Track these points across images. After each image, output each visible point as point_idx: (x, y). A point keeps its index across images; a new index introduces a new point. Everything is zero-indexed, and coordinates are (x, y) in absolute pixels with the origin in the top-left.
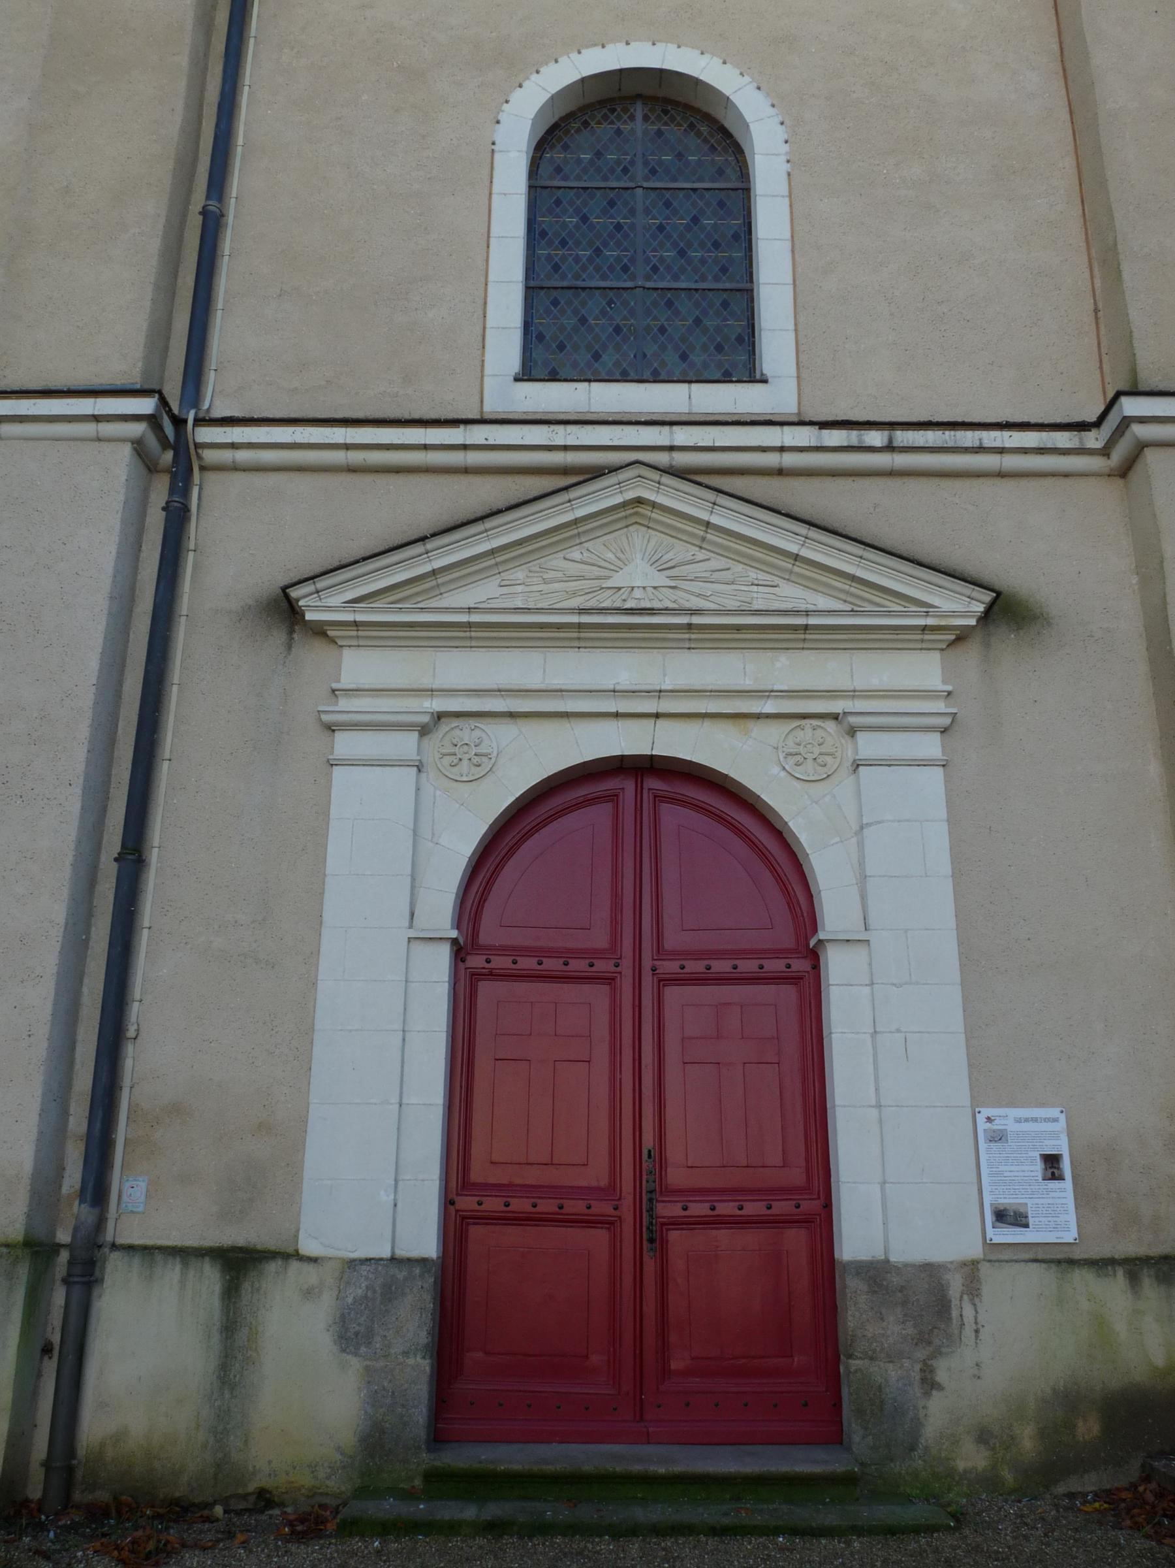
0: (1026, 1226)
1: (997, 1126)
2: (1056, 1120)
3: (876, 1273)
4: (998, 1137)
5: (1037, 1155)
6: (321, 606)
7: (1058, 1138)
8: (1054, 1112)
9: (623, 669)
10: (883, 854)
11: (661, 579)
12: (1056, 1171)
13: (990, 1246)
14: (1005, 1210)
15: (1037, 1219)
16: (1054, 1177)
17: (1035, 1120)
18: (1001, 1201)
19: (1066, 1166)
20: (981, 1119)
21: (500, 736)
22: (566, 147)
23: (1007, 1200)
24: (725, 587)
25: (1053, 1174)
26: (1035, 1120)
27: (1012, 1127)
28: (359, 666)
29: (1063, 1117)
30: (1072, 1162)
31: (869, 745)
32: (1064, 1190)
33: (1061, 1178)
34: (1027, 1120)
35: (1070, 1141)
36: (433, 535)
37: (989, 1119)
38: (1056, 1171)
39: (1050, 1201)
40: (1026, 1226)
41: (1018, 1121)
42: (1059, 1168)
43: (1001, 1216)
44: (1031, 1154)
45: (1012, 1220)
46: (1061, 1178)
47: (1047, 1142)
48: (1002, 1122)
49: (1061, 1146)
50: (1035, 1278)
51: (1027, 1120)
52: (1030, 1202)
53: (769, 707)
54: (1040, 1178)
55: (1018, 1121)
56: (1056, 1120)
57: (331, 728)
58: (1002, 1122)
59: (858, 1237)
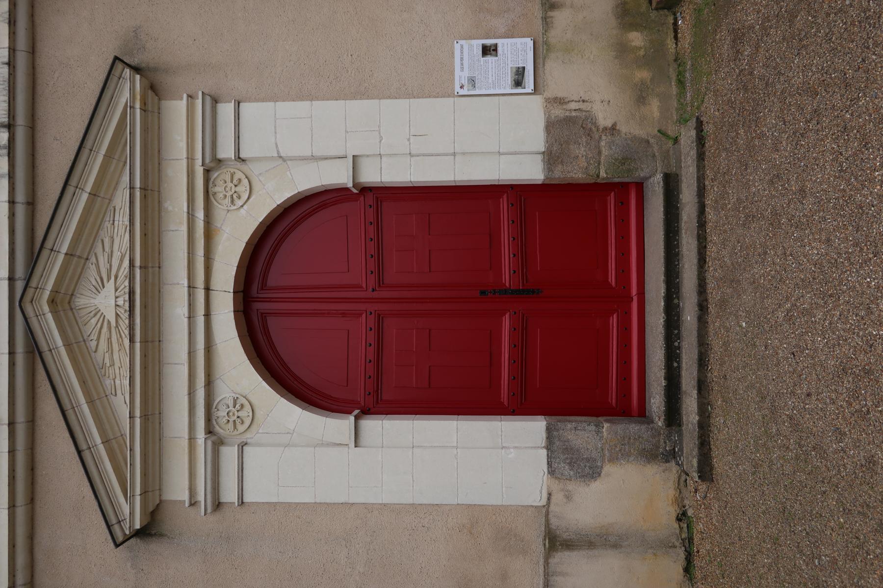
2: (462, 46)
3: (551, 158)
4: (472, 81)
6: (131, 513)
8: (457, 47)
9: (176, 310)
10: (299, 142)
11: (110, 286)
13: (536, 90)
16: (496, 50)
17: (462, 59)
19: (489, 42)
20: (462, 92)
21: (224, 392)
23: (509, 79)
24: (118, 240)
26: (462, 59)
27: (466, 74)
28: (177, 489)
29: (461, 42)
31: (226, 151)
34: (462, 64)
40: (524, 68)
41: (462, 69)
43: (518, 83)
47: (475, 52)
49: (477, 44)
53: (200, 215)
55: (462, 69)
56: (462, 46)
57: (218, 505)
59: (532, 172)
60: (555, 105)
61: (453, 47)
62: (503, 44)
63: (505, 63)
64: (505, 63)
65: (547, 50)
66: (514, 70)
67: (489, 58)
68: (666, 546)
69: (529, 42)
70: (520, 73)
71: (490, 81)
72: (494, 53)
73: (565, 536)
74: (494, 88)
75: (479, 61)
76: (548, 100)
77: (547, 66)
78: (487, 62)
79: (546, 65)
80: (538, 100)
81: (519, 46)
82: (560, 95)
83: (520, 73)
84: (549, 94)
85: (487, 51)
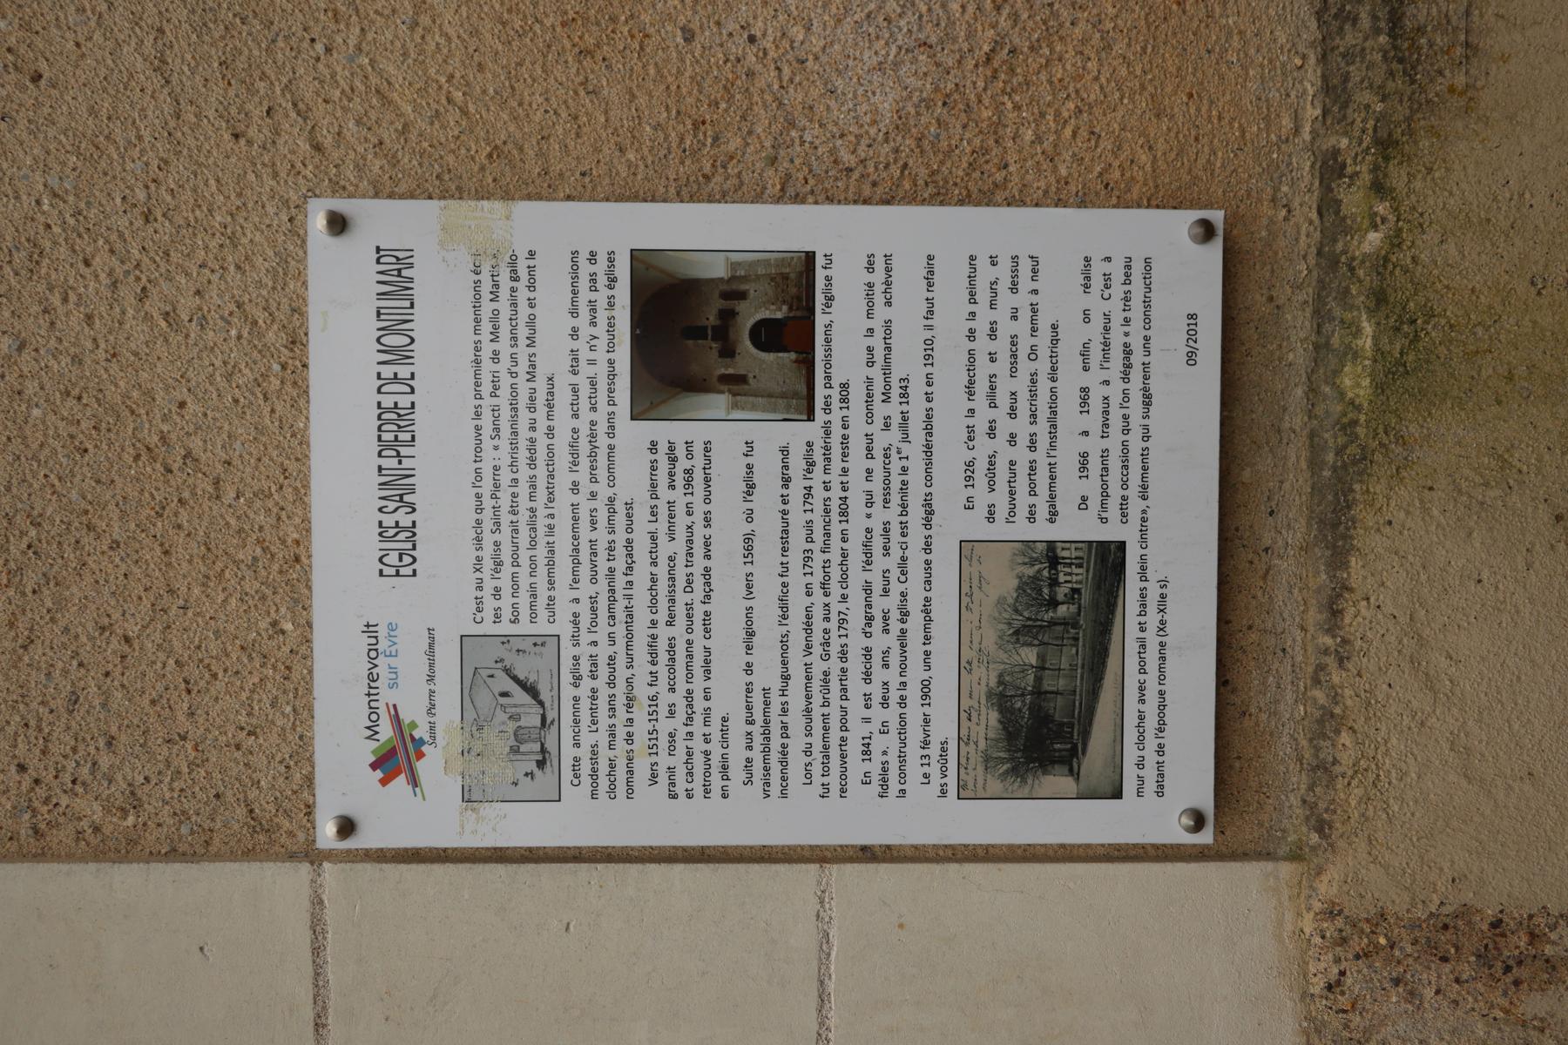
0: (1108, 560)
1: (432, 699)
2: (396, 275)
4: (517, 701)
5: (635, 435)
7: (520, 270)
8: (339, 284)
12: (751, 314)
13: (1236, 816)
14: (1001, 698)
15: (1070, 487)
16: (793, 333)
17: (395, 428)
18: (945, 726)
19: (714, 233)
20: (394, 817)
22: (1305, 549)
23: (941, 682)
25: (768, 336)
26: (395, 428)
27: (443, 599)
29: (387, 221)
30: (693, 191)
32: (880, 266)
33: (798, 279)
34: (397, 489)
35: (545, 188)
36: (784, 663)
37: (395, 759)
38: (751, 314)
39: (950, 376)
40: (1108, 560)
41: (400, 549)
42: (732, 291)
43: (1043, 731)
44: (632, 480)
45: (1069, 657)
46: (798, 279)
47: (553, 353)
48: (411, 661)
49: (586, 243)
50: (1422, 559)
51: (397, 489)
52: (957, 524)
54: (799, 433)
55: (400, 549)
56: (396, 275)
58: (411, 661)
60: (1429, 977)
61: (290, 269)
62: (880, 266)
63: (894, 492)
64: (894, 492)
65: (1391, 373)
66: (1003, 582)
67: (722, 434)
68: (795, 395)
69: (1182, 269)
70: (1067, 605)
71: (727, 698)
72: (769, 366)
73: (719, 270)
74: (772, 779)
75: (596, 454)
76: (1358, 936)
77: (1382, 568)
78: (684, 473)
79: (1370, 541)
80: (1248, 889)
81: (1061, 298)
82: (1504, 887)
83: (1067, 605)
84: (1363, 874)
85: (706, 338)
